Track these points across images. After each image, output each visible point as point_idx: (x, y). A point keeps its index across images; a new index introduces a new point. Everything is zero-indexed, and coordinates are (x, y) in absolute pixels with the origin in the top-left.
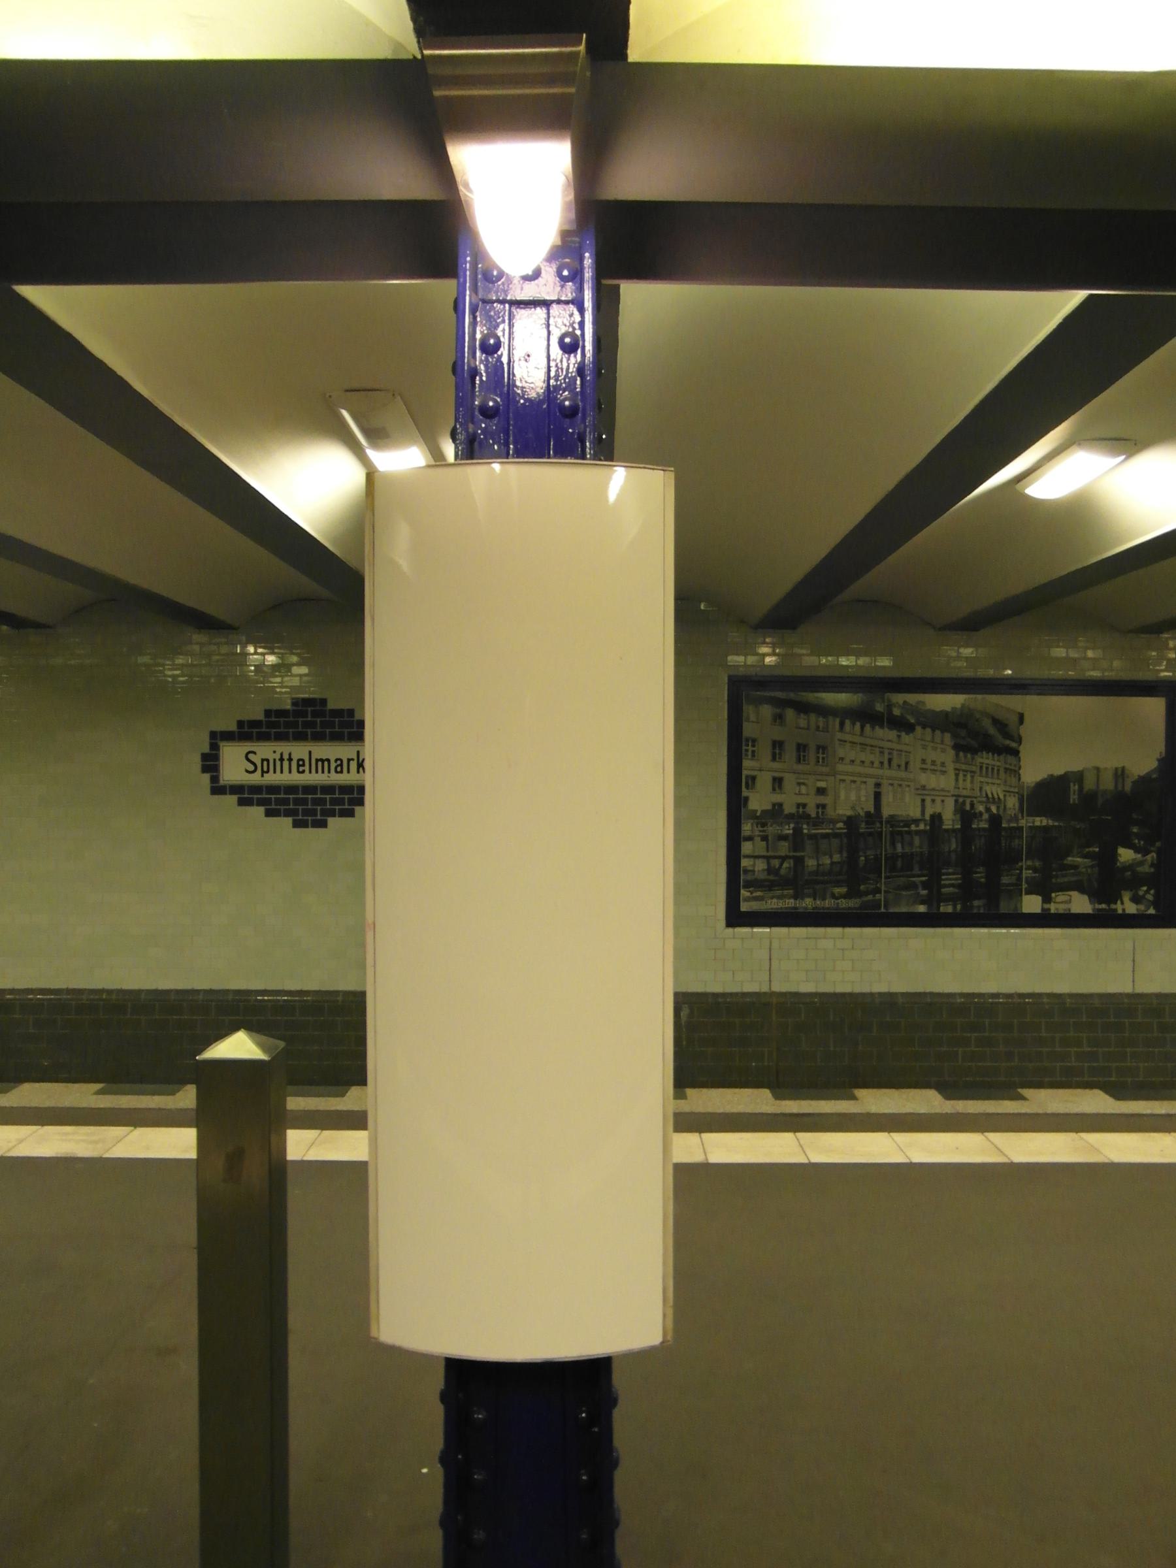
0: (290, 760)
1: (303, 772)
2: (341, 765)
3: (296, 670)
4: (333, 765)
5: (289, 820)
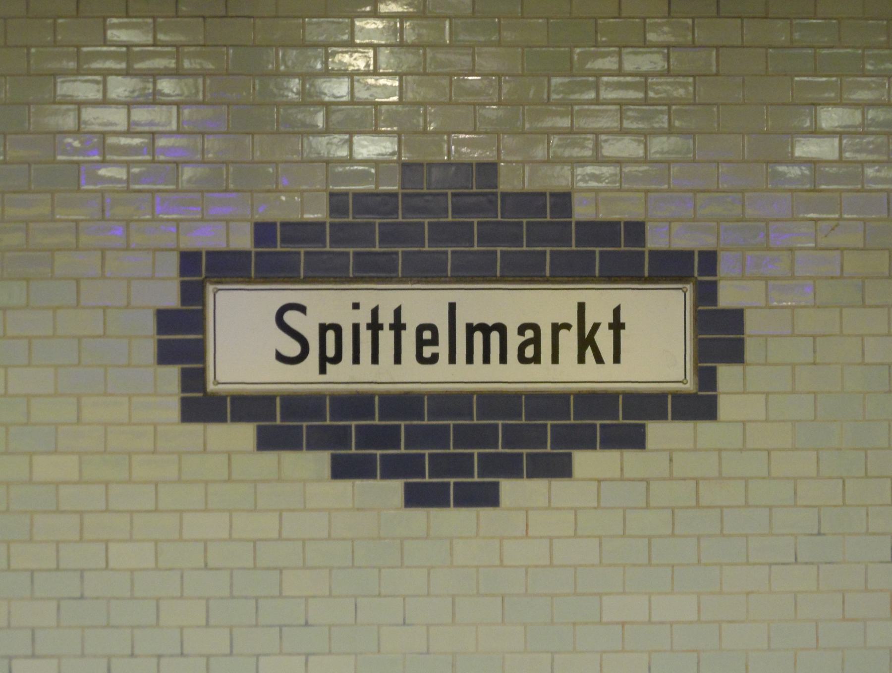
0: (398, 327)
1: (434, 359)
2: (536, 341)
3: (613, 148)
4: (514, 341)
5: (396, 487)
